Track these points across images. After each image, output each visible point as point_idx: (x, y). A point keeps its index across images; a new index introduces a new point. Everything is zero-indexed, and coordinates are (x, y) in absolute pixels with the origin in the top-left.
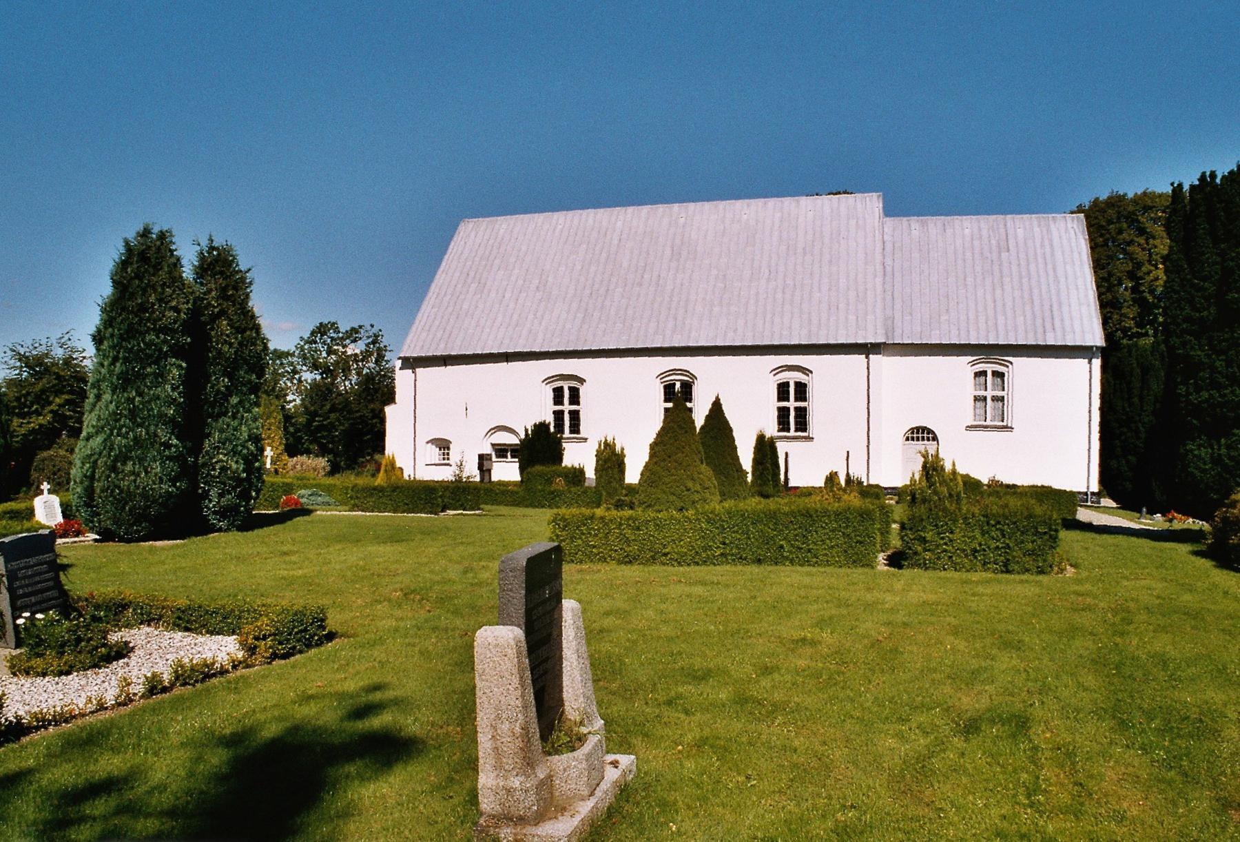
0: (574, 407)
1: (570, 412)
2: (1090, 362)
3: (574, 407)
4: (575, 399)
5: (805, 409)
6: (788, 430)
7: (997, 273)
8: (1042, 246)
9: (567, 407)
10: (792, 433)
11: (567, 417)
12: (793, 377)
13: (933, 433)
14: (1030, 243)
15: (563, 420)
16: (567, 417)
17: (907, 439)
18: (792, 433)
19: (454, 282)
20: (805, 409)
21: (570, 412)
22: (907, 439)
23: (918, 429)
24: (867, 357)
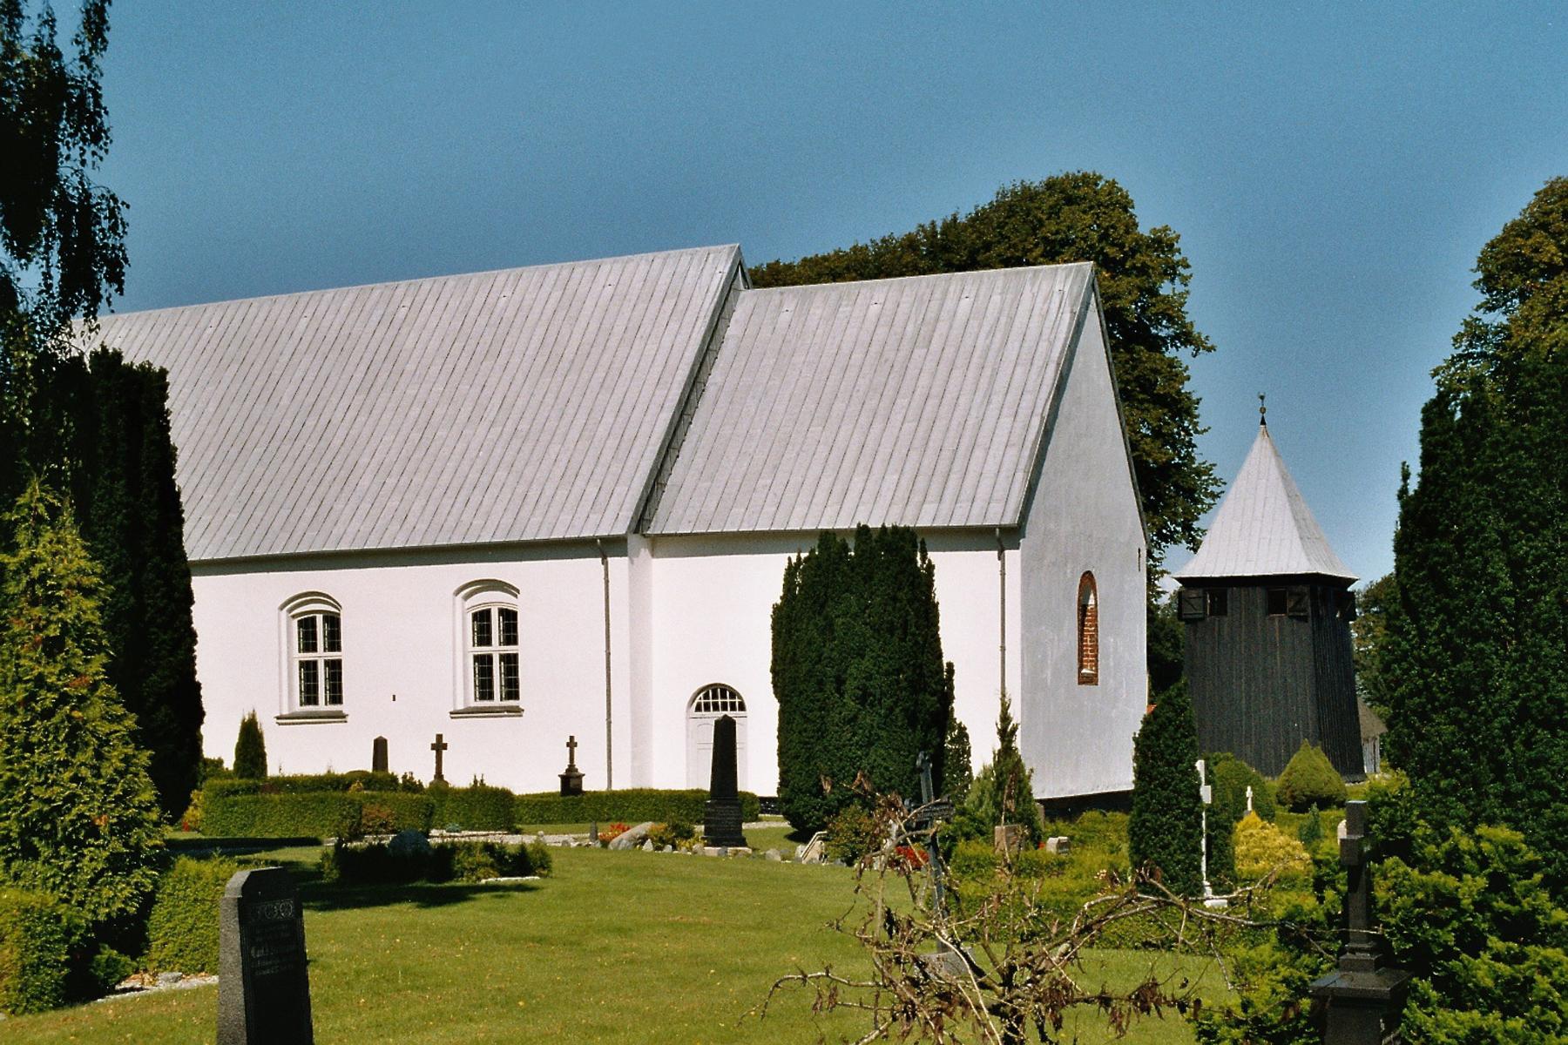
0: (333, 655)
1: (327, 663)
2: (1001, 557)
3: (333, 655)
4: (510, 636)
5: (515, 656)
6: (491, 697)
7: (889, 392)
8: (992, 333)
9: (496, 649)
10: (497, 702)
11: (497, 667)
12: (494, 600)
13: (734, 694)
14: (974, 324)
15: (490, 672)
16: (497, 667)
17: (698, 709)
18: (497, 702)
19: (845, 349)
20: (515, 656)
21: (327, 663)
22: (698, 709)
23: (714, 687)
24: (605, 563)
